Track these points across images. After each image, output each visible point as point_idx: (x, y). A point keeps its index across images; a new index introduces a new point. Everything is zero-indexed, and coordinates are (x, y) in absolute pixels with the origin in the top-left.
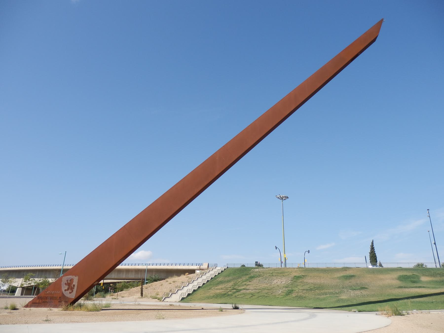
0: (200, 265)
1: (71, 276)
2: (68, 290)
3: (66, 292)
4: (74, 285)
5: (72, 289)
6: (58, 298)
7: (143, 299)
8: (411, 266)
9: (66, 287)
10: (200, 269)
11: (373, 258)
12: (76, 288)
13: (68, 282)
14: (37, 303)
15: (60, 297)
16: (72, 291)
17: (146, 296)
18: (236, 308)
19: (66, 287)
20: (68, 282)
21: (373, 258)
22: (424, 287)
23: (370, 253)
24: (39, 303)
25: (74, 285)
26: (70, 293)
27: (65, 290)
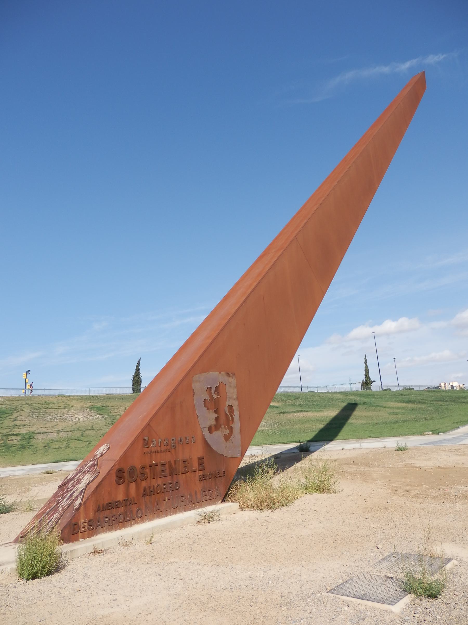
5: (229, 419)
6: (196, 465)
13: (212, 397)
16: (231, 429)
20: (212, 397)
23: (134, 377)
24: (127, 502)
25: (231, 407)
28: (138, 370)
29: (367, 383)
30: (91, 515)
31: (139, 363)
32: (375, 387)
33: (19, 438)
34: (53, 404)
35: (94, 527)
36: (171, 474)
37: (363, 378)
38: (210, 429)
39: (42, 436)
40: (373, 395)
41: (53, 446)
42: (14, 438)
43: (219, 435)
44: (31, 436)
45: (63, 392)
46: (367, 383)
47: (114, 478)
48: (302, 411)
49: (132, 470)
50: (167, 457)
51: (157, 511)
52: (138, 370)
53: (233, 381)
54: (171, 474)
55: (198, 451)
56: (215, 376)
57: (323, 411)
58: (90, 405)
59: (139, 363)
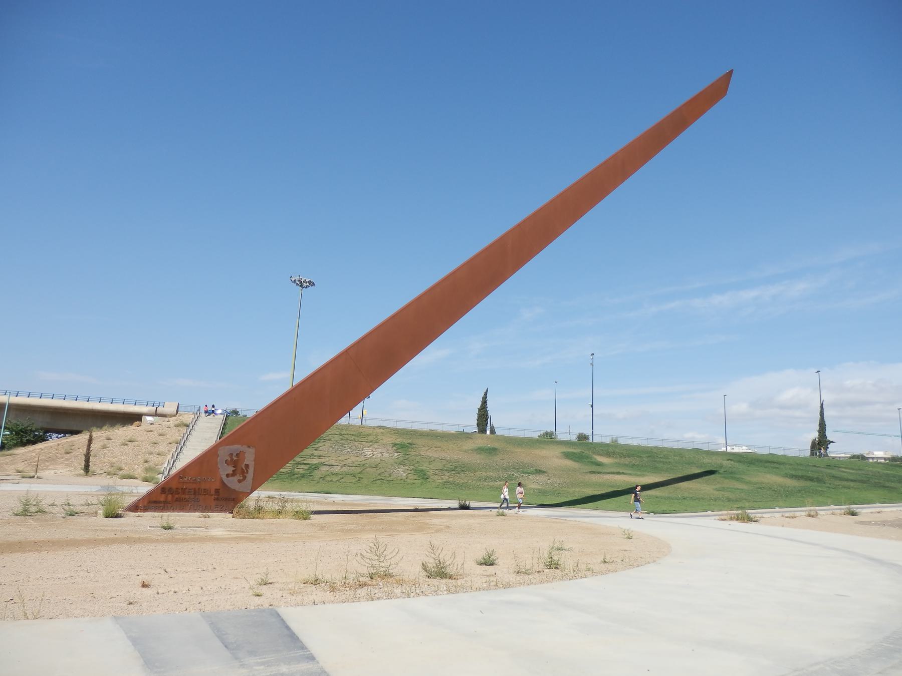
0: (156, 405)
1: (239, 446)
2: (234, 474)
3: (231, 478)
4: (247, 466)
5: (244, 473)
6: (213, 492)
7: (89, 479)
8: (536, 435)
9: (230, 469)
10: (156, 414)
11: (483, 417)
12: (251, 470)
13: (232, 459)
14: (160, 502)
15: (217, 491)
16: (245, 478)
17: (94, 474)
18: (464, 507)
19: (230, 469)
20: (232, 459)
21: (483, 417)
22: (623, 473)
23: (479, 410)
24: (166, 502)
25: (247, 466)
26: (240, 481)
27: (228, 476)
28: (484, 402)
29: (821, 443)
30: (145, 503)
31: (486, 394)
32: (833, 451)
33: (306, 467)
34: (364, 436)
35: (146, 509)
36: (195, 494)
37: (815, 435)
38: (228, 476)
39: (327, 468)
40: (836, 464)
41: (328, 478)
42: (303, 466)
43: (235, 479)
44: (316, 467)
45: (384, 424)
46: (821, 443)
47: (160, 491)
48: (618, 473)
49: (170, 489)
50: (193, 486)
51: (182, 509)
52: (484, 402)
53: (252, 450)
54: (195, 494)
55: (217, 485)
56: (237, 448)
57: (643, 476)
58: (399, 441)
59: (486, 394)
